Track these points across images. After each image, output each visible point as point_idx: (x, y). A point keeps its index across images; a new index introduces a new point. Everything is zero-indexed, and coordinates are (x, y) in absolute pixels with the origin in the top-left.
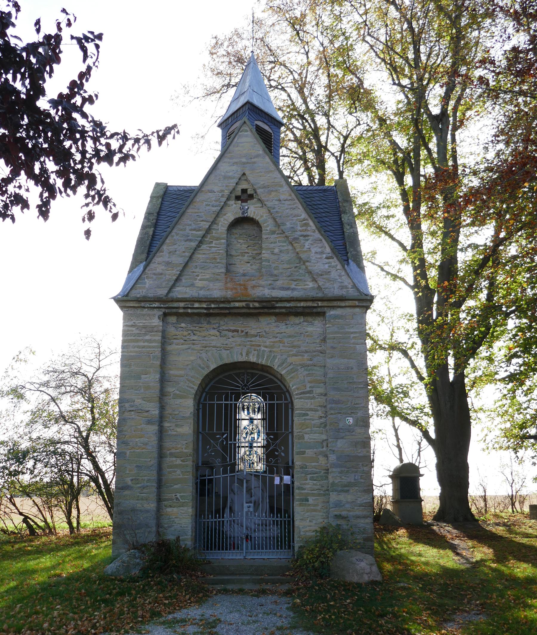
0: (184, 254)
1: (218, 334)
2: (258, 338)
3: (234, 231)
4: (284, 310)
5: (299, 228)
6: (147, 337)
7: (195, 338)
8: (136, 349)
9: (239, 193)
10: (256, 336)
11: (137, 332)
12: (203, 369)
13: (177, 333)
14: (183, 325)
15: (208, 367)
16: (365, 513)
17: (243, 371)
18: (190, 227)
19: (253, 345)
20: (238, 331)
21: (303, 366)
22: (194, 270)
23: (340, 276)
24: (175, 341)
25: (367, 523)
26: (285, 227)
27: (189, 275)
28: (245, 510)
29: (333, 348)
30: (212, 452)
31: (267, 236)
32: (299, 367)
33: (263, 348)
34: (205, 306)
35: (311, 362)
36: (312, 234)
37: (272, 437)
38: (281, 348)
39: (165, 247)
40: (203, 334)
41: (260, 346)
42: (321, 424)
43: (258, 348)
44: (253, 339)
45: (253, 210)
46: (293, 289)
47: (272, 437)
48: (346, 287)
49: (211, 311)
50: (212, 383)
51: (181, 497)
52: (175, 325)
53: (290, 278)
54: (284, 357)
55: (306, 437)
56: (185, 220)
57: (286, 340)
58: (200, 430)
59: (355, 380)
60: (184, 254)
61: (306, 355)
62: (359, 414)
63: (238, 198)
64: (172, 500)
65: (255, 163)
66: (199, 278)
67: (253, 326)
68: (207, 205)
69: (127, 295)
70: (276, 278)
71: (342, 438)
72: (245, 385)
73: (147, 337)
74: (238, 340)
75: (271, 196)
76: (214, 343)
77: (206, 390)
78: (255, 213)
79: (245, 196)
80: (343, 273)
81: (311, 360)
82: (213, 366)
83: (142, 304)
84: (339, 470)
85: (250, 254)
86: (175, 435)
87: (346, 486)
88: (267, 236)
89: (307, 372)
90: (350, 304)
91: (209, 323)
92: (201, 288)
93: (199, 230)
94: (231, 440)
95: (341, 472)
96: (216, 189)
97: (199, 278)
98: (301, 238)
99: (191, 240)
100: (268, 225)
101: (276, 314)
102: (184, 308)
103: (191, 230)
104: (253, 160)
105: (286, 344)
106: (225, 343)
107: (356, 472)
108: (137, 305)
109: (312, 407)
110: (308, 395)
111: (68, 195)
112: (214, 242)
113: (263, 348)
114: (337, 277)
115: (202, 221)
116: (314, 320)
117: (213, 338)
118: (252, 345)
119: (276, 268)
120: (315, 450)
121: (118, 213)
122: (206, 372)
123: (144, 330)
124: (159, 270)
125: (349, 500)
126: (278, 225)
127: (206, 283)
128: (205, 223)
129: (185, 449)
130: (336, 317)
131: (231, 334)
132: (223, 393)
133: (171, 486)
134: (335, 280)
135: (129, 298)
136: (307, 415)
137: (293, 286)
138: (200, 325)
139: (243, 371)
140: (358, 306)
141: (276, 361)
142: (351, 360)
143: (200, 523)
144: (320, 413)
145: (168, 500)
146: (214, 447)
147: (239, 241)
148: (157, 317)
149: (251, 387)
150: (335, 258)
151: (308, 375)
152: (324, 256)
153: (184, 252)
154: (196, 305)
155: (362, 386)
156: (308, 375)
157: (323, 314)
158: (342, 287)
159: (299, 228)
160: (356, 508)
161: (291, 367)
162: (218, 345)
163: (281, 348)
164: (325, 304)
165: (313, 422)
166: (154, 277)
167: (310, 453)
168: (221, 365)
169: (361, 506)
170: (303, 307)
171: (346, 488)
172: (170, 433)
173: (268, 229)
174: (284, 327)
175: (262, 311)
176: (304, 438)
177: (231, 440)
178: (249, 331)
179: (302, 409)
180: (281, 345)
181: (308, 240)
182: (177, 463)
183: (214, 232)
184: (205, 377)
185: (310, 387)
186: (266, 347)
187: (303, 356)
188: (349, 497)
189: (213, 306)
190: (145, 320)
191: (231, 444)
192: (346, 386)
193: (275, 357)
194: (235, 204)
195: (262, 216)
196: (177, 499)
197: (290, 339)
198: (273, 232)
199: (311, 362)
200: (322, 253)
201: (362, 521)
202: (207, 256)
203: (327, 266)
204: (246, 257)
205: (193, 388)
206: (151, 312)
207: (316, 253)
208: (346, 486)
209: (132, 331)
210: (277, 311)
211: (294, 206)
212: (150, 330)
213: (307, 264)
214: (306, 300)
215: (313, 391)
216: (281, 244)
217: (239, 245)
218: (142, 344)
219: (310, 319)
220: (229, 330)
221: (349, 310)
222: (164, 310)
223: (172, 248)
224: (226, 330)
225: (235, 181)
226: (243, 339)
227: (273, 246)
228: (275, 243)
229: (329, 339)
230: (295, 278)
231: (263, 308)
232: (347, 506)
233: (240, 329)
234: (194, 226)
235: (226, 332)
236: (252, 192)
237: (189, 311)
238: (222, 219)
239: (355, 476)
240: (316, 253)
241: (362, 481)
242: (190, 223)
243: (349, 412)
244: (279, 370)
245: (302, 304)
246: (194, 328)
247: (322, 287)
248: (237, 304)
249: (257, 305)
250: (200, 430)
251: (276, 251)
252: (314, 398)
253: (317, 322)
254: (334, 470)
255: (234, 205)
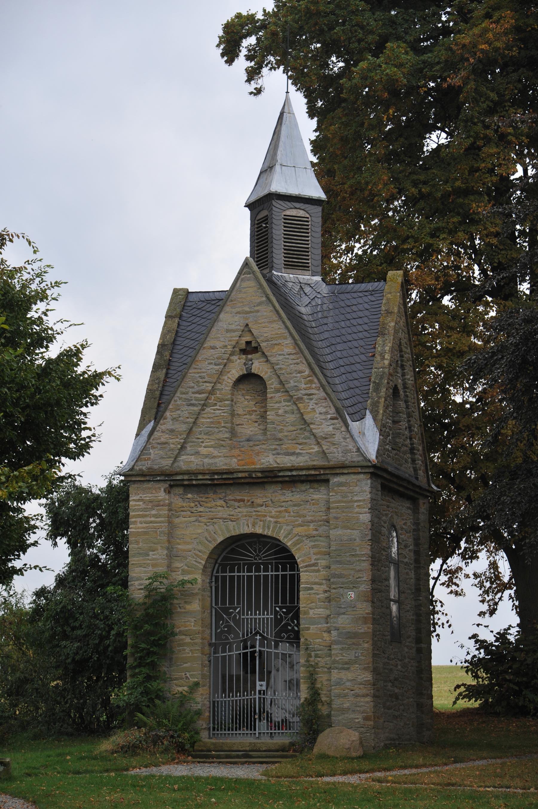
0: (188, 420)
1: (224, 504)
2: (264, 507)
3: (241, 386)
4: (287, 479)
5: (303, 386)
6: (153, 512)
7: (201, 509)
8: (144, 525)
9: (243, 346)
10: (262, 506)
11: (144, 506)
12: (210, 542)
13: (184, 505)
14: (190, 496)
15: (215, 540)
16: (365, 691)
17: (255, 540)
18: (193, 390)
19: (260, 515)
20: (243, 501)
21: (309, 537)
22: (199, 436)
23: (345, 438)
24: (182, 513)
25: (367, 702)
26: (289, 385)
27: (193, 442)
28: (258, 688)
29: (336, 518)
30: (224, 627)
31: (272, 395)
32: (304, 539)
33: (269, 519)
34: (207, 477)
35: (317, 532)
36: (317, 392)
37: (284, 610)
38: (287, 518)
39: (168, 414)
40: (209, 505)
41: (266, 516)
42: (326, 598)
43: (263, 519)
44: (259, 509)
45: (258, 366)
46: (299, 454)
47: (284, 610)
48: (350, 451)
49: (216, 482)
50: (224, 554)
51: (191, 675)
52: (181, 496)
53: (294, 442)
54: (289, 528)
55: (311, 612)
56: (189, 382)
57: (291, 509)
58: (214, 605)
59: (358, 553)
60: (188, 420)
61: (312, 525)
62: (360, 589)
63: (244, 352)
64: (182, 679)
65: (258, 311)
66: (203, 445)
67: (259, 496)
68: (209, 364)
69: (132, 469)
70: (281, 442)
71: (344, 614)
72: (258, 555)
73: (153, 512)
74: (244, 510)
75: (274, 351)
76: (220, 515)
77: (219, 561)
78: (259, 369)
79: (250, 349)
80: (348, 436)
81: (316, 530)
82: (220, 539)
83: (148, 478)
84: (339, 646)
85: (258, 412)
86: (184, 612)
87: (346, 663)
88: (272, 395)
89: (313, 544)
90: (352, 471)
91: (215, 493)
92: (206, 456)
93: (203, 393)
94: (243, 615)
95: (342, 649)
96: (218, 344)
97: (203, 445)
98: (305, 397)
99: (193, 405)
100: (272, 384)
101: (281, 482)
102: (188, 480)
103: (193, 393)
104: (256, 308)
105: (292, 513)
106: (232, 513)
107: (357, 649)
108: (142, 479)
109: (317, 580)
110: (313, 568)
111: (75, 346)
112: (218, 404)
113: (269, 519)
114: (342, 440)
115: (206, 382)
116: (321, 486)
117: (220, 508)
118: (257, 516)
119: (281, 431)
120: (320, 626)
121: (230, 62)
122: (212, 546)
123: (150, 504)
124: (163, 440)
125: (350, 678)
126: (281, 383)
127: (208, 455)
128: (208, 384)
129: (194, 626)
130: (341, 484)
131: (237, 504)
132: (236, 564)
133: (181, 665)
134: (339, 444)
135: (133, 473)
136: (312, 589)
137: (298, 451)
138: (206, 496)
139: (255, 540)
140: (360, 473)
141: (282, 531)
142: (354, 531)
143: (214, 702)
144: (325, 587)
145: (176, 679)
146: (227, 622)
147: (247, 397)
148: (162, 489)
149: (264, 557)
150: (340, 419)
151: (313, 547)
152: (329, 416)
153: (188, 418)
154: (200, 477)
155: (364, 558)
156: (313, 547)
157: (327, 481)
158: (346, 452)
159: (303, 386)
160: (356, 686)
161: (297, 538)
162: (225, 516)
163: (287, 518)
164: (327, 472)
165: (318, 597)
166: (159, 446)
167: (313, 629)
168: (228, 538)
169: (361, 684)
170: (305, 475)
171: (346, 666)
172: (179, 610)
173: (272, 386)
174: (290, 494)
175: (266, 480)
176: (309, 614)
177: (243, 615)
178: (255, 501)
179: (307, 583)
180: (287, 514)
181: (311, 399)
182: (187, 641)
183: (218, 392)
184: (211, 553)
185: (315, 559)
186: (272, 517)
187: (309, 526)
188: (350, 675)
189: (216, 477)
190: (152, 493)
191: (243, 619)
192: (348, 559)
193: (280, 528)
194: (239, 359)
195: (266, 373)
196: (187, 677)
197: (296, 508)
198: (277, 391)
199: (317, 532)
200: (326, 413)
201: (362, 700)
202: (212, 420)
203: (331, 428)
204: (253, 416)
205: (200, 563)
206: (157, 485)
207: (320, 413)
208: (346, 663)
209: (139, 505)
210: (280, 479)
211: (298, 361)
212: (157, 504)
213: (312, 426)
214: (308, 469)
215: (317, 563)
216: (287, 403)
217: (246, 403)
218: (148, 519)
219: (316, 485)
220: (235, 500)
221: (353, 476)
222: (169, 483)
223: (175, 414)
224: (232, 500)
225: (238, 333)
226: (249, 509)
227: (278, 406)
228: (280, 402)
229: (334, 508)
230: (301, 441)
231: (266, 477)
232: (348, 684)
233: (246, 498)
234: (196, 389)
235: (233, 502)
236: (256, 345)
237: (194, 482)
238: (225, 378)
239: (356, 653)
240: (320, 413)
241: (363, 658)
242: (193, 385)
243: (351, 586)
244: (285, 541)
245: (304, 473)
246: (201, 499)
247: (326, 451)
248: (240, 475)
249: (259, 475)
250: (214, 605)
251: (280, 412)
252: (318, 571)
253: (323, 488)
254: (335, 647)
255: (239, 361)
